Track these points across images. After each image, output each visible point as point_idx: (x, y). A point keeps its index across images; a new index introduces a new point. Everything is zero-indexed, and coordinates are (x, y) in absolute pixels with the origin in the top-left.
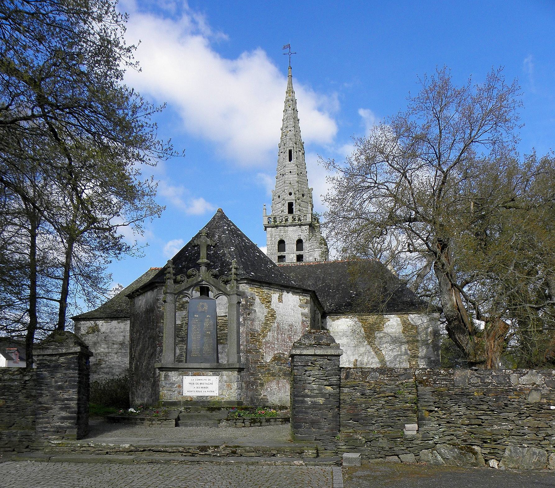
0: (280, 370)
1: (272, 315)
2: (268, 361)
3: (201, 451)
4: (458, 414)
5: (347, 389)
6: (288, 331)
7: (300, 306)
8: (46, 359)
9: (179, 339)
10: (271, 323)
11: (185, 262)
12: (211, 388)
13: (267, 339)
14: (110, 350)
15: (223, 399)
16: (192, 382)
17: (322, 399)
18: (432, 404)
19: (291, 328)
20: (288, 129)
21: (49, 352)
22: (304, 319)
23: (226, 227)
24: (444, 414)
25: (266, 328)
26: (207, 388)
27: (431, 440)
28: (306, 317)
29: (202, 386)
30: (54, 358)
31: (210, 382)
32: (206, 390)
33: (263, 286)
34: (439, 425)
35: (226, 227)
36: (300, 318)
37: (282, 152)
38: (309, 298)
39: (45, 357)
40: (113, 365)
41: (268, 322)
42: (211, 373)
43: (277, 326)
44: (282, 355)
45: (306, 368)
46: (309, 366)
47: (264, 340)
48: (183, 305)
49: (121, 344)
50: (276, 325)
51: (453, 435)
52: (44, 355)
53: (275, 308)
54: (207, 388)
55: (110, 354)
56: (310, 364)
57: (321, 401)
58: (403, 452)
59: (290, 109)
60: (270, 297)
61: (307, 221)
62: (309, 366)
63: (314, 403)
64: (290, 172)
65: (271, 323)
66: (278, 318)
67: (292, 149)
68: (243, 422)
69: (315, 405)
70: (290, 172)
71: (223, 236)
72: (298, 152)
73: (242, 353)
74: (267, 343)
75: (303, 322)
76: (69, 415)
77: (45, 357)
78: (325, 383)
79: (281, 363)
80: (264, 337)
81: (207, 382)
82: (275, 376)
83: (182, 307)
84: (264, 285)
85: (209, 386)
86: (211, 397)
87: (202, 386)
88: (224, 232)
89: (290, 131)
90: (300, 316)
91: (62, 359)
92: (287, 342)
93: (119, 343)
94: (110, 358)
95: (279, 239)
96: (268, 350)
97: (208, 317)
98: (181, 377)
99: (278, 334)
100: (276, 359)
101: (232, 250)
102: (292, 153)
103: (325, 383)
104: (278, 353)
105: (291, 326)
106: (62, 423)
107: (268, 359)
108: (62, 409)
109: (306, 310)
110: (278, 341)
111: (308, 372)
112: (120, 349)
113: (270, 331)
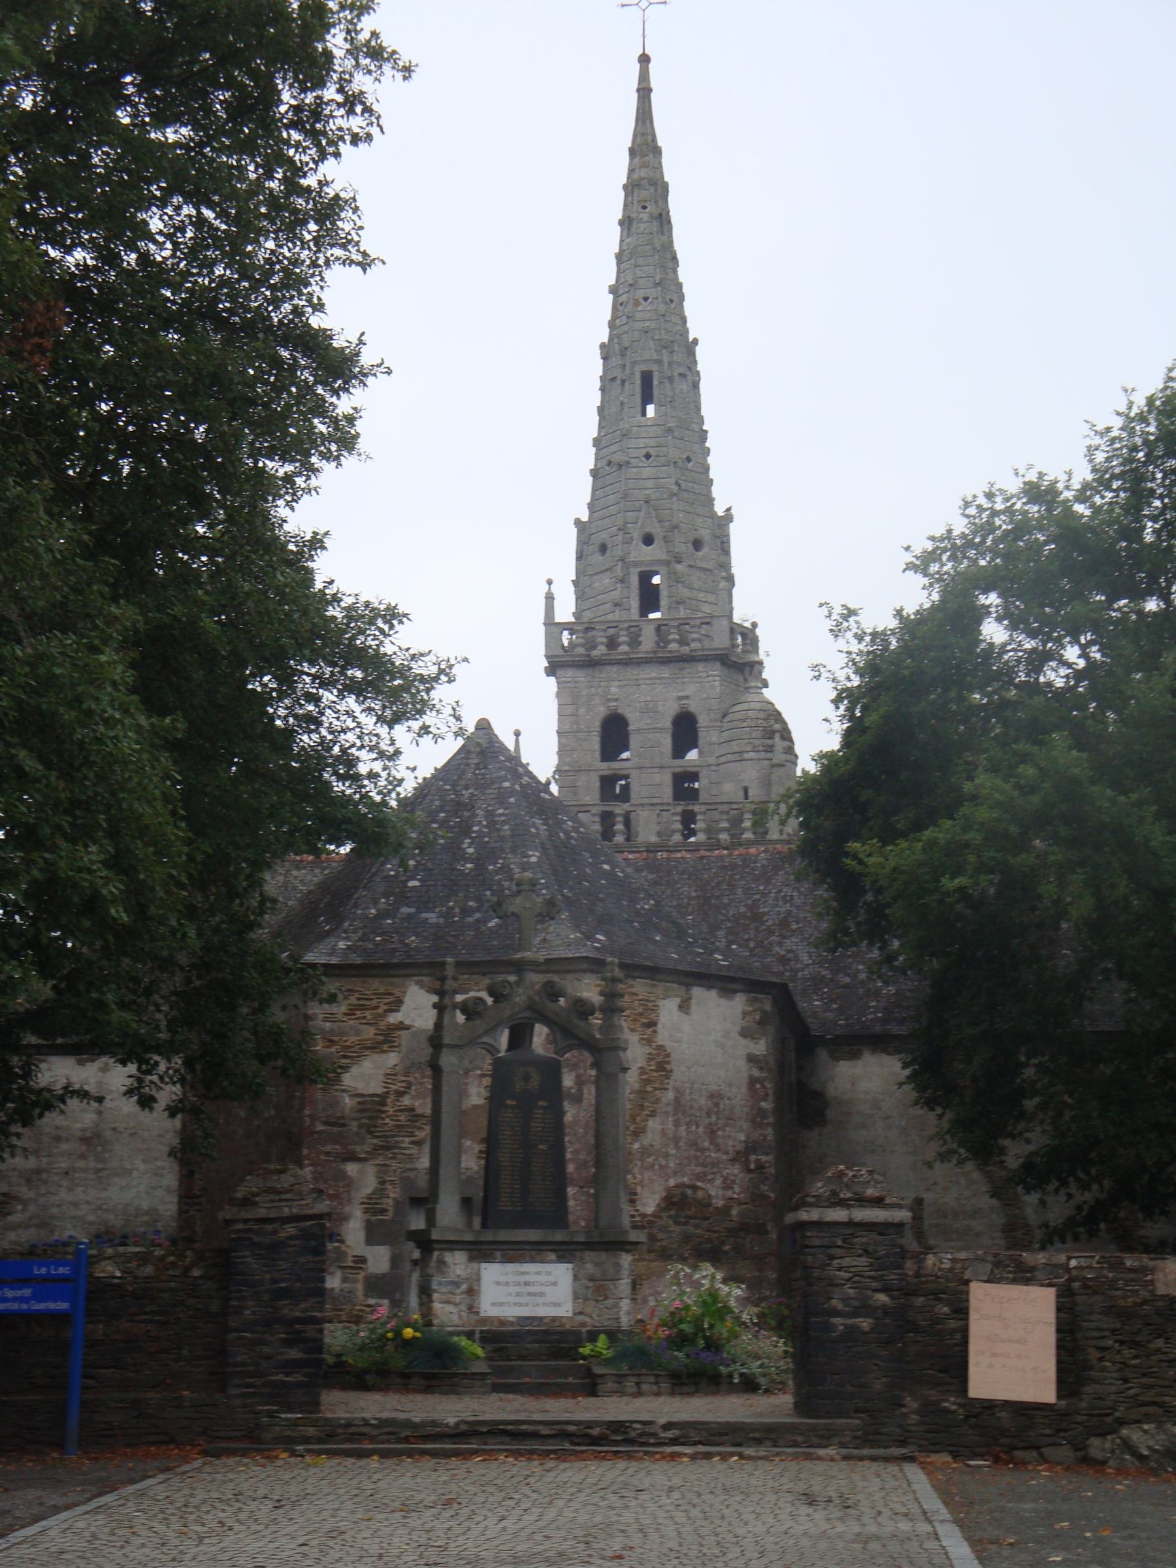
0: (686, 1238)
1: (661, 1064)
2: (650, 1210)
3: (615, 1432)
4: (1163, 1357)
5: (921, 1299)
6: (709, 1115)
7: (745, 1033)
8: (250, 1230)
9: (375, 1141)
10: (656, 1089)
11: (387, 898)
12: (552, 1294)
13: (647, 1139)
14: (45, 1160)
15: (583, 1324)
16: (503, 1279)
17: (869, 1320)
18: (1107, 1333)
19: (717, 1105)
20: (640, 294)
21: (262, 1213)
22: (756, 1073)
23: (506, 784)
24: (1136, 1357)
25: (642, 1107)
26: (542, 1294)
27: (1108, 1415)
28: (761, 1069)
29: (530, 1289)
30: (269, 1227)
31: (551, 1279)
32: (540, 1300)
33: (634, 978)
34: (1126, 1381)
35: (506, 784)
36: (742, 1071)
37: (614, 379)
38: (768, 1007)
39: (250, 1226)
40: (52, 1217)
41: (649, 1089)
42: (553, 1256)
43: (677, 1100)
44: (689, 1192)
45: (832, 1251)
46: (839, 1247)
47: (636, 1146)
48: (387, 1035)
49: (85, 1140)
50: (671, 1095)
51: (1155, 1403)
52: (246, 1221)
53: (669, 1045)
54: (542, 1294)
55: (44, 1176)
56: (840, 1243)
57: (865, 1324)
58: (1050, 1440)
59: (645, 216)
60: (655, 1009)
61: (716, 644)
62: (839, 1247)
63: (852, 1330)
64: (648, 456)
65: (656, 1089)
66: (680, 1074)
67: (654, 367)
68: (657, 1383)
69: (852, 1334)
70: (648, 456)
71: (501, 811)
72: (677, 379)
73: (574, 1186)
74: (645, 1152)
75: (752, 1081)
76: (305, 1356)
77: (250, 1226)
78: (874, 1285)
79: (688, 1217)
80: (636, 1134)
81: (542, 1278)
82: (671, 1256)
83: (384, 1042)
84: (636, 974)
85: (549, 1290)
86: (554, 1319)
87: (530, 1289)
88: (501, 800)
89: (646, 299)
90: (742, 1064)
91: (290, 1230)
92: (703, 1150)
93: (79, 1134)
94: (43, 1191)
95: (602, 711)
96: (648, 1174)
97: (542, 1107)
98: (475, 1265)
99: (677, 1124)
100: (673, 1204)
101: (533, 859)
102: (655, 382)
103: (874, 1285)
104: (677, 1186)
105: (716, 1097)
106: (287, 1374)
107: (649, 1204)
108: (289, 1343)
109: (760, 1047)
110: (677, 1147)
111: (835, 1262)
112: (83, 1157)
113: (653, 1114)
